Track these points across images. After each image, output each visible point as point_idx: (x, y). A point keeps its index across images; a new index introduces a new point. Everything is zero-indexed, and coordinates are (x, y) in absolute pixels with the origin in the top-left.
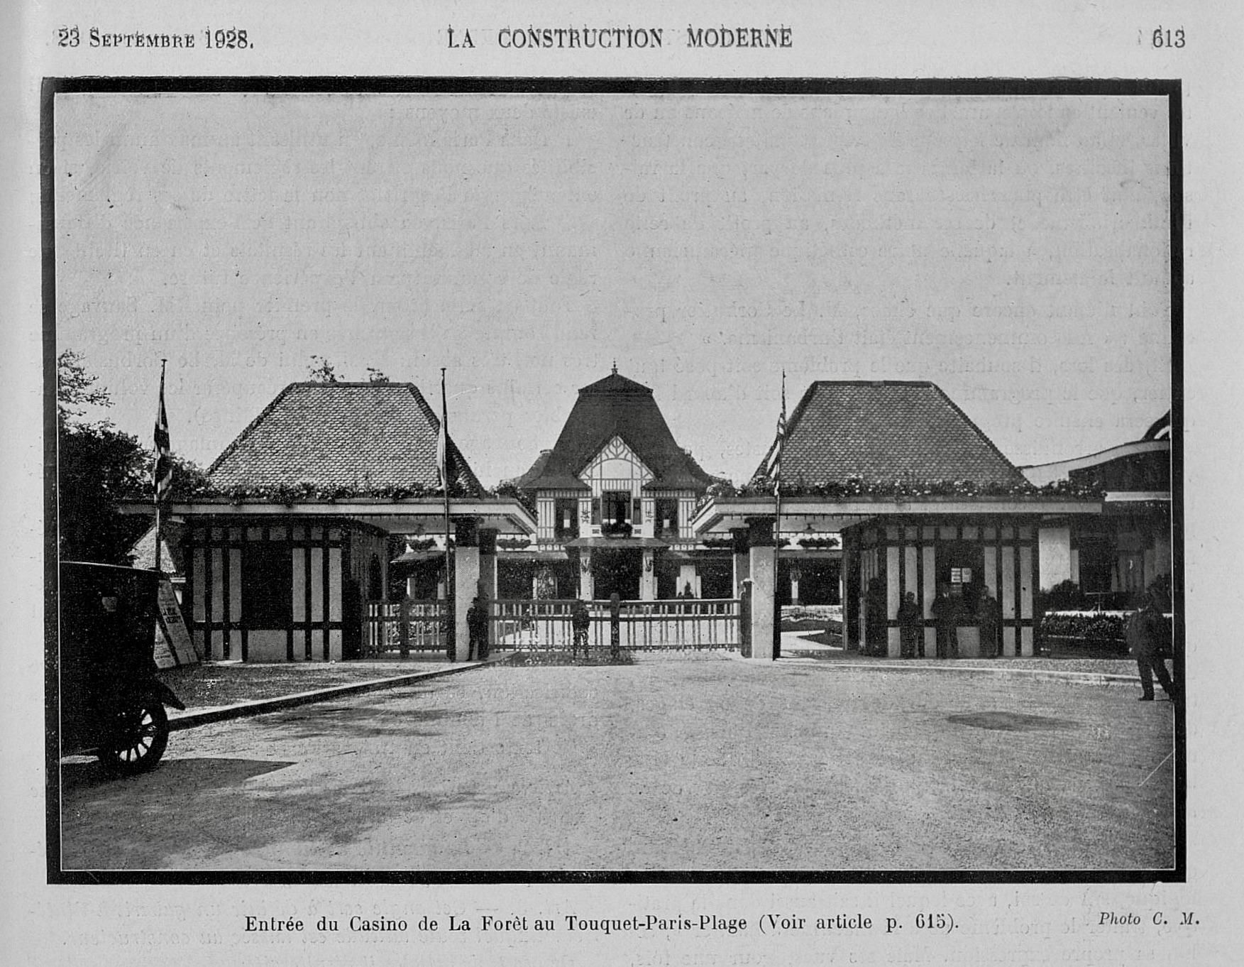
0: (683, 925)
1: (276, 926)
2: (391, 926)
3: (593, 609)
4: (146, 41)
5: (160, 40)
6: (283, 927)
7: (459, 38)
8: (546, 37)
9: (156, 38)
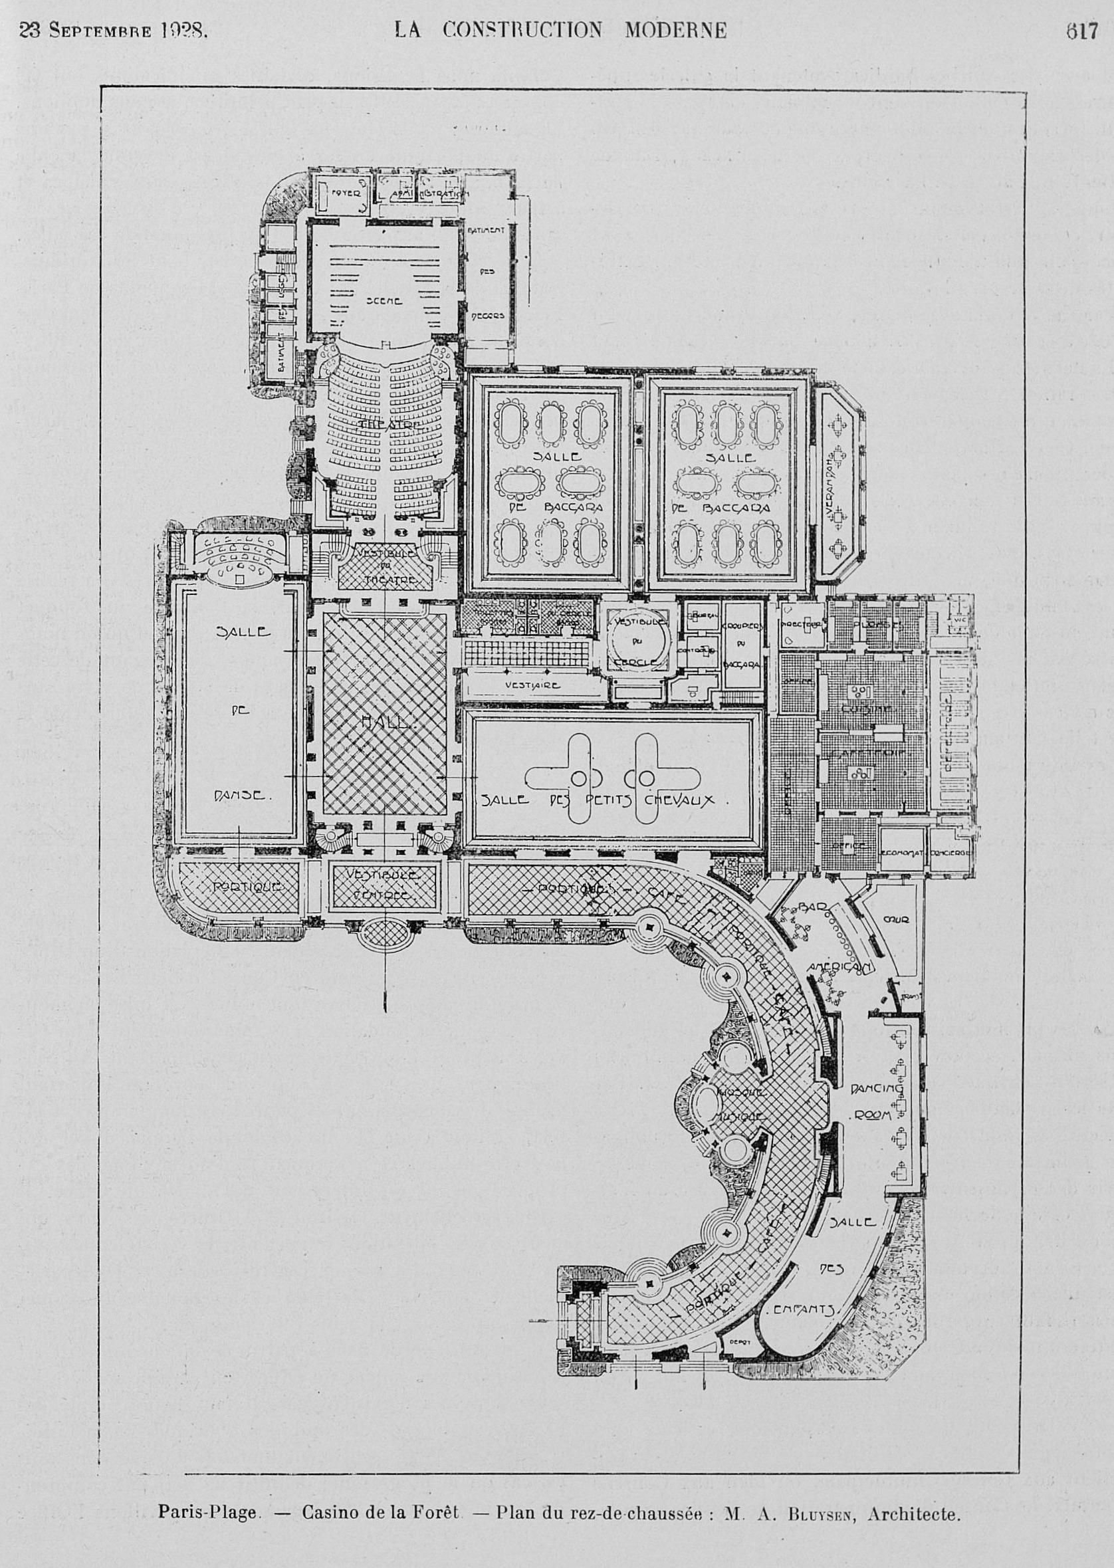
0: (194, 1514)
2: (344, 1513)
4: (103, 31)
5: (117, 31)
7: (405, 28)
8: (490, 28)
9: (114, 29)
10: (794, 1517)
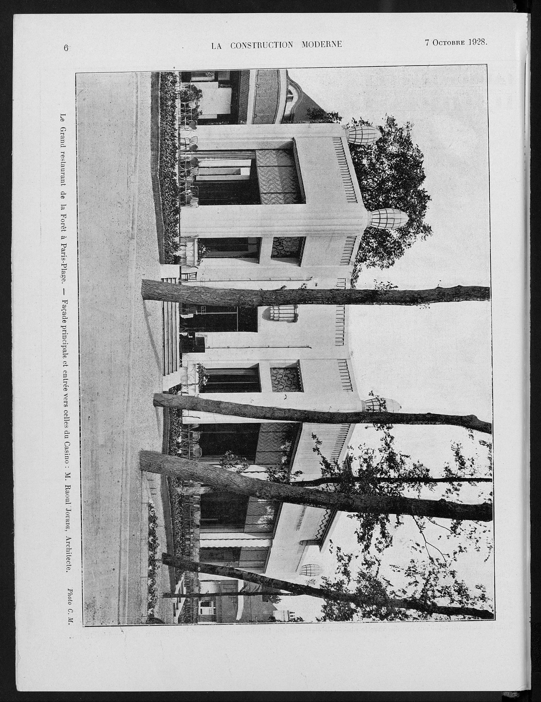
1: (65, 381)
2: (65, 376)
3: (202, 250)
6: (65, 383)
10: (67, 487)
